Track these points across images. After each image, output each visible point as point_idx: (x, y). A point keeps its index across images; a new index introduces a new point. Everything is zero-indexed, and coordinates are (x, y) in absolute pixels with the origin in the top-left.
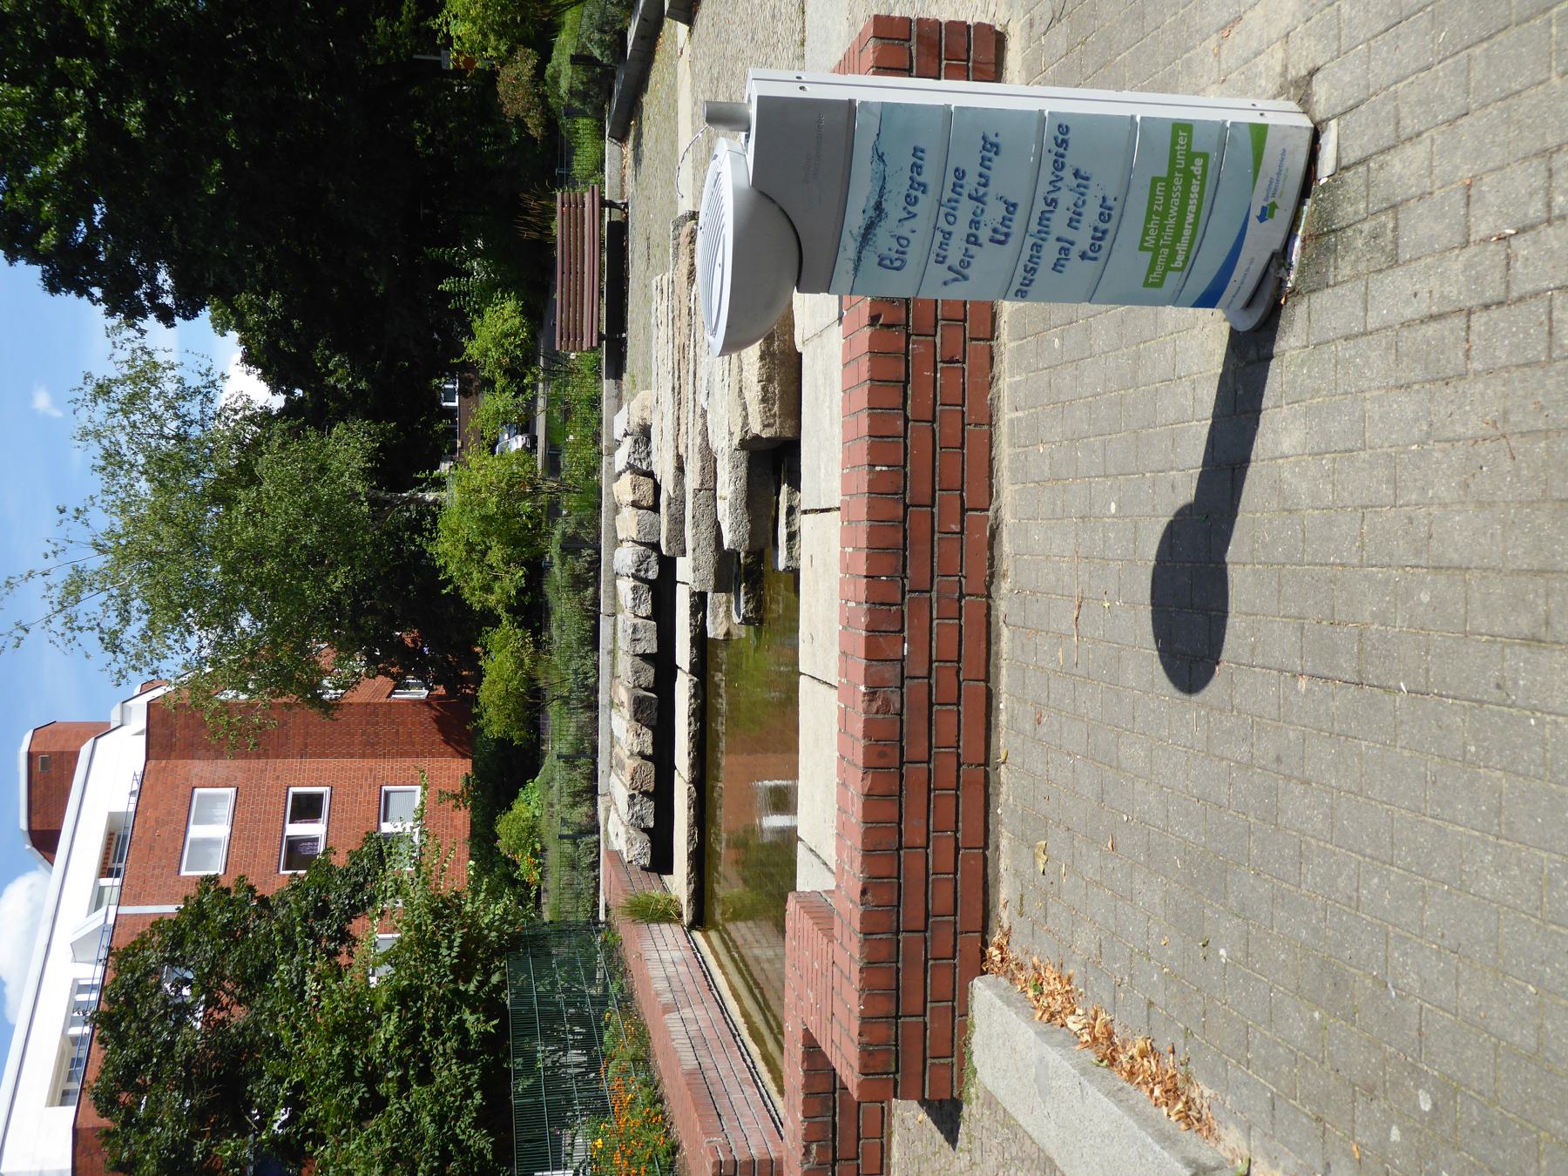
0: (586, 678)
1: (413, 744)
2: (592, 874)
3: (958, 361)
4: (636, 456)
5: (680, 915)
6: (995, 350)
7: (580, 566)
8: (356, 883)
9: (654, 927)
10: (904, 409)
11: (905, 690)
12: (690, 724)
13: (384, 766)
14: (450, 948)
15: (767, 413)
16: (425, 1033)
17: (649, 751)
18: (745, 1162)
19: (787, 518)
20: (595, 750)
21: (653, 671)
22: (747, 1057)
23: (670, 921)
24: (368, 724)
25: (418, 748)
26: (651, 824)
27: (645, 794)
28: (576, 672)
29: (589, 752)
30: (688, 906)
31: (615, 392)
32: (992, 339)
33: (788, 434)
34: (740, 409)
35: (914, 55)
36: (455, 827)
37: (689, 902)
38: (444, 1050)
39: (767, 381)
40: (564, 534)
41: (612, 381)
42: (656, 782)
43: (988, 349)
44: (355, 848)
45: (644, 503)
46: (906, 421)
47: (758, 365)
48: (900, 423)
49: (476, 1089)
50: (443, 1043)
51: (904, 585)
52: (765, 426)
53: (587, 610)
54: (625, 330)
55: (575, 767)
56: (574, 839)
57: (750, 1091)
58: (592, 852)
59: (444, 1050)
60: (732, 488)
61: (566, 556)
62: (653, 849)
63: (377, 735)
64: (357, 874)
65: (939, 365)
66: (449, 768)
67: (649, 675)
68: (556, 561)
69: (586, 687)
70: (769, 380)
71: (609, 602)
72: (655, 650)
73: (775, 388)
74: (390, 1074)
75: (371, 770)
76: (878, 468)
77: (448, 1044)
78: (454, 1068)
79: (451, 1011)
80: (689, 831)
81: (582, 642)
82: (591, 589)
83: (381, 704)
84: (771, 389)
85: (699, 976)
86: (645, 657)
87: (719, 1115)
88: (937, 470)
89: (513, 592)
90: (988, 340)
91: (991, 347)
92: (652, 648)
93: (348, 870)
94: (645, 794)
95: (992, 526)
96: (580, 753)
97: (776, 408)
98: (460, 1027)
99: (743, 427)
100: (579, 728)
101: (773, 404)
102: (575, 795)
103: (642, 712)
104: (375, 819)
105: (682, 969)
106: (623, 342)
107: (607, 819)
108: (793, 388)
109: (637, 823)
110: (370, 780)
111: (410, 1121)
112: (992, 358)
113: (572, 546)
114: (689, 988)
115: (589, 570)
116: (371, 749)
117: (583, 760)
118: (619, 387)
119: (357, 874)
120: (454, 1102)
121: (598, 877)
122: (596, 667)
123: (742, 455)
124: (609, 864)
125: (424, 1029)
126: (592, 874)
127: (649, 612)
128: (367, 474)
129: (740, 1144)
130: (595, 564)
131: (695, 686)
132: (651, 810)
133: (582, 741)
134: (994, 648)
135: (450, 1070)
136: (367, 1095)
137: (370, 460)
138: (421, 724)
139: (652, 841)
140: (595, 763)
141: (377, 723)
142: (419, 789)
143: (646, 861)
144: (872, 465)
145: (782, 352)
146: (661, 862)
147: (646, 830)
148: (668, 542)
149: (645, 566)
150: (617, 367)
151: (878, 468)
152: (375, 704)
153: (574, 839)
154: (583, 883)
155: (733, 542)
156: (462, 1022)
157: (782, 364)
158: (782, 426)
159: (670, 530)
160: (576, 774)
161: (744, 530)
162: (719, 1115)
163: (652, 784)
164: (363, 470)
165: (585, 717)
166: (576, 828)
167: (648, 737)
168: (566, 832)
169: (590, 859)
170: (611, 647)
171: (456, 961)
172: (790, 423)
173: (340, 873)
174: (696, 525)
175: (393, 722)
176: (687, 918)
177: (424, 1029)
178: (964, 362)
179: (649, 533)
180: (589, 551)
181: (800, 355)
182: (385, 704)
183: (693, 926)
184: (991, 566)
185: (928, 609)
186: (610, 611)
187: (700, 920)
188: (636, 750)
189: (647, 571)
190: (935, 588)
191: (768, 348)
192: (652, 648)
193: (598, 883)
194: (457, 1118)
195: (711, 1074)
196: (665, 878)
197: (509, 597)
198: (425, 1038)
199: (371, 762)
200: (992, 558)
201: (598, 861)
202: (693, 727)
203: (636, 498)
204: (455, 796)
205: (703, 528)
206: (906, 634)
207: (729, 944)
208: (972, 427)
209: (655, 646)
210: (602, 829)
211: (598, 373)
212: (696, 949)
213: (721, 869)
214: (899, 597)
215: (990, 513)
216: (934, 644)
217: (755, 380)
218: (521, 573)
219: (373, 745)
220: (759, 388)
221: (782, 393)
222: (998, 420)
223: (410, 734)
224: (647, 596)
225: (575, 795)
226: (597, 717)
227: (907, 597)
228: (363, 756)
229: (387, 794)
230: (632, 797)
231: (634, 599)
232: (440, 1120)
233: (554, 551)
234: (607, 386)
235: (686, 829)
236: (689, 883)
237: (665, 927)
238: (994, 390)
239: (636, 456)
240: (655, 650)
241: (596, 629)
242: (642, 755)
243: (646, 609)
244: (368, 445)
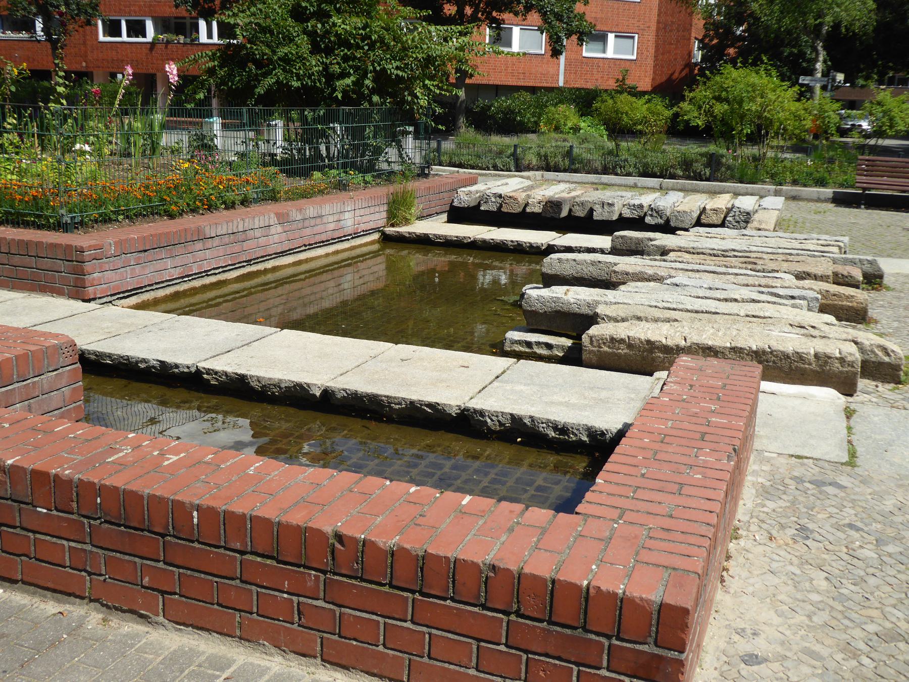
0: (620, 168)
1: (663, 54)
2: (490, 166)
3: (300, 619)
4: (737, 213)
5: (393, 225)
6: (312, 661)
7: (698, 167)
8: (562, 16)
9: (385, 207)
10: (252, 553)
11: (9, 502)
12: (512, 241)
13: (651, 36)
14: (397, 68)
15: (602, 341)
16: (346, 51)
17: (528, 210)
18: (83, 269)
19: (543, 343)
20: (576, 171)
21: (582, 215)
22: (221, 270)
23: (389, 218)
24: (679, 25)
25: (660, 57)
26: (482, 208)
27: (501, 206)
28: (626, 160)
29: (573, 167)
30: (395, 232)
31: (822, 197)
32: (323, 660)
33: (585, 356)
34: (623, 315)
35: (638, 647)
36: (607, 80)
37: (398, 232)
38: (334, 64)
39: (630, 344)
40: (722, 156)
41: (831, 196)
42: (508, 213)
43: (313, 653)
44: (587, 17)
45: (703, 217)
46: (242, 553)
47: (643, 338)
48: (238, 546)
49: (302, 84)
50: (338, 63)
51: (95, 519)
52: (591, 338)
53: (666, 170)
54: (867, 208)
55: (564, 157)
56: (514, 154)
57: (176, 273)
58: (504, 166)
59: (334, 64)
60: (572, 301)
61: (706, 157)
62: (463, 208)
63: (671, 31)
64: (569, 17)
65: (295, 599)
66: (646, 77)
67: (580, 213)
68: (704, 150)
69: (614, 168)
70: (630, 346)
71: (670, 186)
72: (595, 218)
73: (623, 350)
74: (319, 26)
75: (649, 27)
76: (195, 514)
77: (337, 66)
78: (317, 68)
79: (356, 69)
80: (442, 236)
81: (646, 165)
82: (681, 174)
83: (690, 34)
84: (622, 346)
85: (324, 237)
86: (591, 211)
87: (145, 251)
88: (196, 574)
89: (686, 118)
90: (322, 656)
91: (315, 657)
92: (597, 216)
93: (572, 12)
94: (501, 206)
95: (150, 618)
96: (572, 161)
97: (606, 349)
98: (343, 75)
99: (607, 316)
100: (589, 161)
101: (609, 347)
102: (546, 156)
103: (551, 207)
104: (616, 30)
105: (332, 226)
106: (858, 206)
107: (522, 177)
108: (624, 365)
109: (485, 198)
110: (642, 27)
111: (290, 40)
112: (304, 655)
113: (713, 161)
114: (308, 231)
115: (694, 172)
116: (663, 27)
117: (567, 162)
118: (826, 200)
119: (569, 17)
120: (295, 69)
121: (489, 169)
122: (629, 174)
123: (193, 370)
124: (468, 176)
125: (349, 51)
126: (490, 166)
127: (624, 215)
128: (836, 26)
129: (107, 265)
130: (699, 177)
131: (538, 247)
132: (491, 209)
133: (581, 162)
134: (49, 594)
135: (315, 66)
136: (308, 12)
137: (847, 29)
138: (675, 59)
139: (469, 208)
140: (565, 171)
141: (678, 31)
142: (634, 57)
143: (456, 204)
144: (198, 508)
145: (653, 360)
146: (457, 215)
147: (479, 205)
148: (622, 237)
149: (655, 214)
150: (841, 200)
151: (195, 514)
152: (691, 29)
153: (514, 154)
154: (485, 161)
155: (530, 297)
156: (348, 75)
157: (644, 358)
158: (591, 352)
159: (631, 239)
160: (559, 159)
161: (538, 307)
162: (145, 251)
163: (506, 210)
164: (841, 22)
165: (598, 165)
166: (521, 156)
167: (537, 209)
168: (519, 150)
169: (500, 165)
170: (639, 185)
171: (389, 72)
172: (594, 360)
173: (570, 7)
174: (593, 263)
175: (678, 41)
176: (390, 230)
177: (349, 51)
178: (299, 625)
179: (677, 219)
180: (708, 173)
181: (651, 374)
182: (690, 36)
183: (383, 233)
184: (116, 609)
185: (76, 538)
186: (664, 186)
187: (386, 239)
188: (530, 201)
189: (651, 216)
190: (94, 550)
191: (658, 348)
192: (597, 216)
193: (484, 169)
194: (284, 70)
195: (199, 245)
196: (445, 217)
197: (682, 116)
198: (343, 51)
199: (654, 27)
200: (124, 611)
201: (498, 170)
202: (510, 243)
203: (708, 211)
204: (624, 79)
205: (591, 268)
206: (55, 512)
207: (375, 254)
208: (238, 619)
209: (598, 218)
210: (517, 173)
211: (841, 185)
212: (367, 233)
213: (417, 255)
214: (83, 513)
215: (161, 619)
216: (48, 538)
217: (631, 334)
218: (700, 123)
219: (665, 28)
220: (623, 336)
221: (619, 356)
222: (245, 647)
223: (669, 52)
224: (635, 214)
225: (546, 156)
226: (598, 173)
227: (85, 521)
228: (658, 22)
229: (633, 37)
230: (500, 196)
231: (634, 205)
232: (286, 60)
233: (712, 148)
234: (828, 192)
235: (444, 234)
236: (409, 233)
237: (384, 215)
238: (273, 650)
239: (737, 213)
240: (595, 218)
241: (653, 175)
242: (527, 205)
243: (627, 213)
244: (857, 24)
